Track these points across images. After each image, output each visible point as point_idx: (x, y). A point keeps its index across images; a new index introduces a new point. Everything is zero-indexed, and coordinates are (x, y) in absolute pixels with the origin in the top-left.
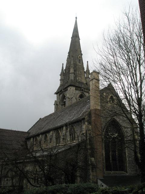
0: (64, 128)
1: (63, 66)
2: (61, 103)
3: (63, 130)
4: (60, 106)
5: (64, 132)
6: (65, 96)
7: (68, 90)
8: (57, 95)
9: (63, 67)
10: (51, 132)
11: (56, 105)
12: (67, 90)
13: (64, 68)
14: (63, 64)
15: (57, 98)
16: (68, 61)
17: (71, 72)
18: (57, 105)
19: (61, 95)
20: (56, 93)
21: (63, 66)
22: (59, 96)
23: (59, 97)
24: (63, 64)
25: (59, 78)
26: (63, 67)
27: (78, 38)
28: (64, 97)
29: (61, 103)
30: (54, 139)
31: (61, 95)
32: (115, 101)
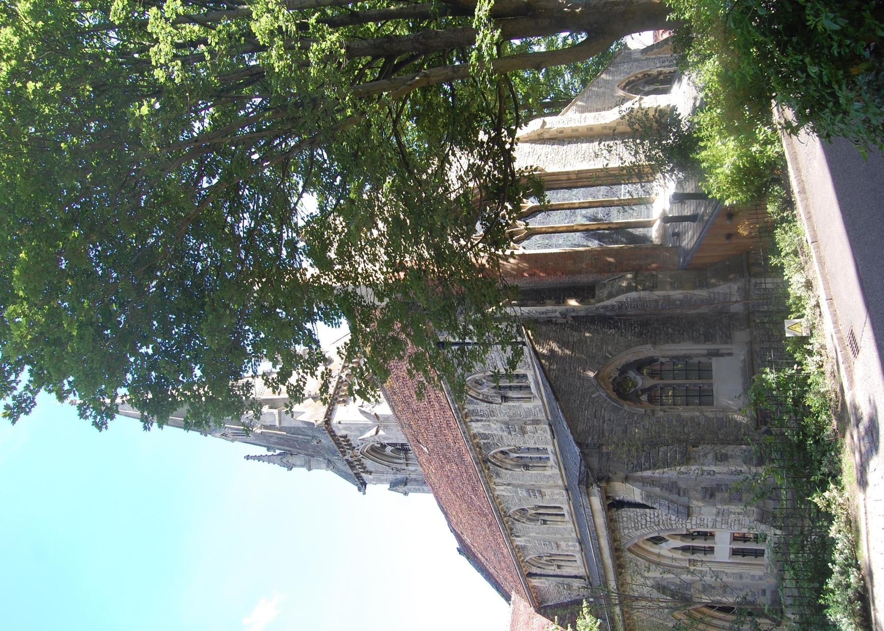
0: (476, 427)
1: (255, 458)
2: (399, 466)
3: (485, 436)
4: (411, 468)
5: (495, 429)
6: (373, 449)
7: (344, 433)
8: (370, 483)
9: (259, 458)
10: (500, 491)
11: (408, 486)
12: (345, 437)
13: (262, 451)
14: (248, 457)
15: (380, 481)
16: (235, 434)
17: (630, 197)
18: (405, 482)
19: (368, 463)
20: (362, 485)
21: (255, 458)
22: (371, 473)
23: (377, 472)
24: (248, 457)
25: (299, 472)
26: (259, 458)
27: (769, 283)
28: (377, 451)
29: (399, 466)
30: (530, 477)
31: (368, 463)
32: (381, 225)
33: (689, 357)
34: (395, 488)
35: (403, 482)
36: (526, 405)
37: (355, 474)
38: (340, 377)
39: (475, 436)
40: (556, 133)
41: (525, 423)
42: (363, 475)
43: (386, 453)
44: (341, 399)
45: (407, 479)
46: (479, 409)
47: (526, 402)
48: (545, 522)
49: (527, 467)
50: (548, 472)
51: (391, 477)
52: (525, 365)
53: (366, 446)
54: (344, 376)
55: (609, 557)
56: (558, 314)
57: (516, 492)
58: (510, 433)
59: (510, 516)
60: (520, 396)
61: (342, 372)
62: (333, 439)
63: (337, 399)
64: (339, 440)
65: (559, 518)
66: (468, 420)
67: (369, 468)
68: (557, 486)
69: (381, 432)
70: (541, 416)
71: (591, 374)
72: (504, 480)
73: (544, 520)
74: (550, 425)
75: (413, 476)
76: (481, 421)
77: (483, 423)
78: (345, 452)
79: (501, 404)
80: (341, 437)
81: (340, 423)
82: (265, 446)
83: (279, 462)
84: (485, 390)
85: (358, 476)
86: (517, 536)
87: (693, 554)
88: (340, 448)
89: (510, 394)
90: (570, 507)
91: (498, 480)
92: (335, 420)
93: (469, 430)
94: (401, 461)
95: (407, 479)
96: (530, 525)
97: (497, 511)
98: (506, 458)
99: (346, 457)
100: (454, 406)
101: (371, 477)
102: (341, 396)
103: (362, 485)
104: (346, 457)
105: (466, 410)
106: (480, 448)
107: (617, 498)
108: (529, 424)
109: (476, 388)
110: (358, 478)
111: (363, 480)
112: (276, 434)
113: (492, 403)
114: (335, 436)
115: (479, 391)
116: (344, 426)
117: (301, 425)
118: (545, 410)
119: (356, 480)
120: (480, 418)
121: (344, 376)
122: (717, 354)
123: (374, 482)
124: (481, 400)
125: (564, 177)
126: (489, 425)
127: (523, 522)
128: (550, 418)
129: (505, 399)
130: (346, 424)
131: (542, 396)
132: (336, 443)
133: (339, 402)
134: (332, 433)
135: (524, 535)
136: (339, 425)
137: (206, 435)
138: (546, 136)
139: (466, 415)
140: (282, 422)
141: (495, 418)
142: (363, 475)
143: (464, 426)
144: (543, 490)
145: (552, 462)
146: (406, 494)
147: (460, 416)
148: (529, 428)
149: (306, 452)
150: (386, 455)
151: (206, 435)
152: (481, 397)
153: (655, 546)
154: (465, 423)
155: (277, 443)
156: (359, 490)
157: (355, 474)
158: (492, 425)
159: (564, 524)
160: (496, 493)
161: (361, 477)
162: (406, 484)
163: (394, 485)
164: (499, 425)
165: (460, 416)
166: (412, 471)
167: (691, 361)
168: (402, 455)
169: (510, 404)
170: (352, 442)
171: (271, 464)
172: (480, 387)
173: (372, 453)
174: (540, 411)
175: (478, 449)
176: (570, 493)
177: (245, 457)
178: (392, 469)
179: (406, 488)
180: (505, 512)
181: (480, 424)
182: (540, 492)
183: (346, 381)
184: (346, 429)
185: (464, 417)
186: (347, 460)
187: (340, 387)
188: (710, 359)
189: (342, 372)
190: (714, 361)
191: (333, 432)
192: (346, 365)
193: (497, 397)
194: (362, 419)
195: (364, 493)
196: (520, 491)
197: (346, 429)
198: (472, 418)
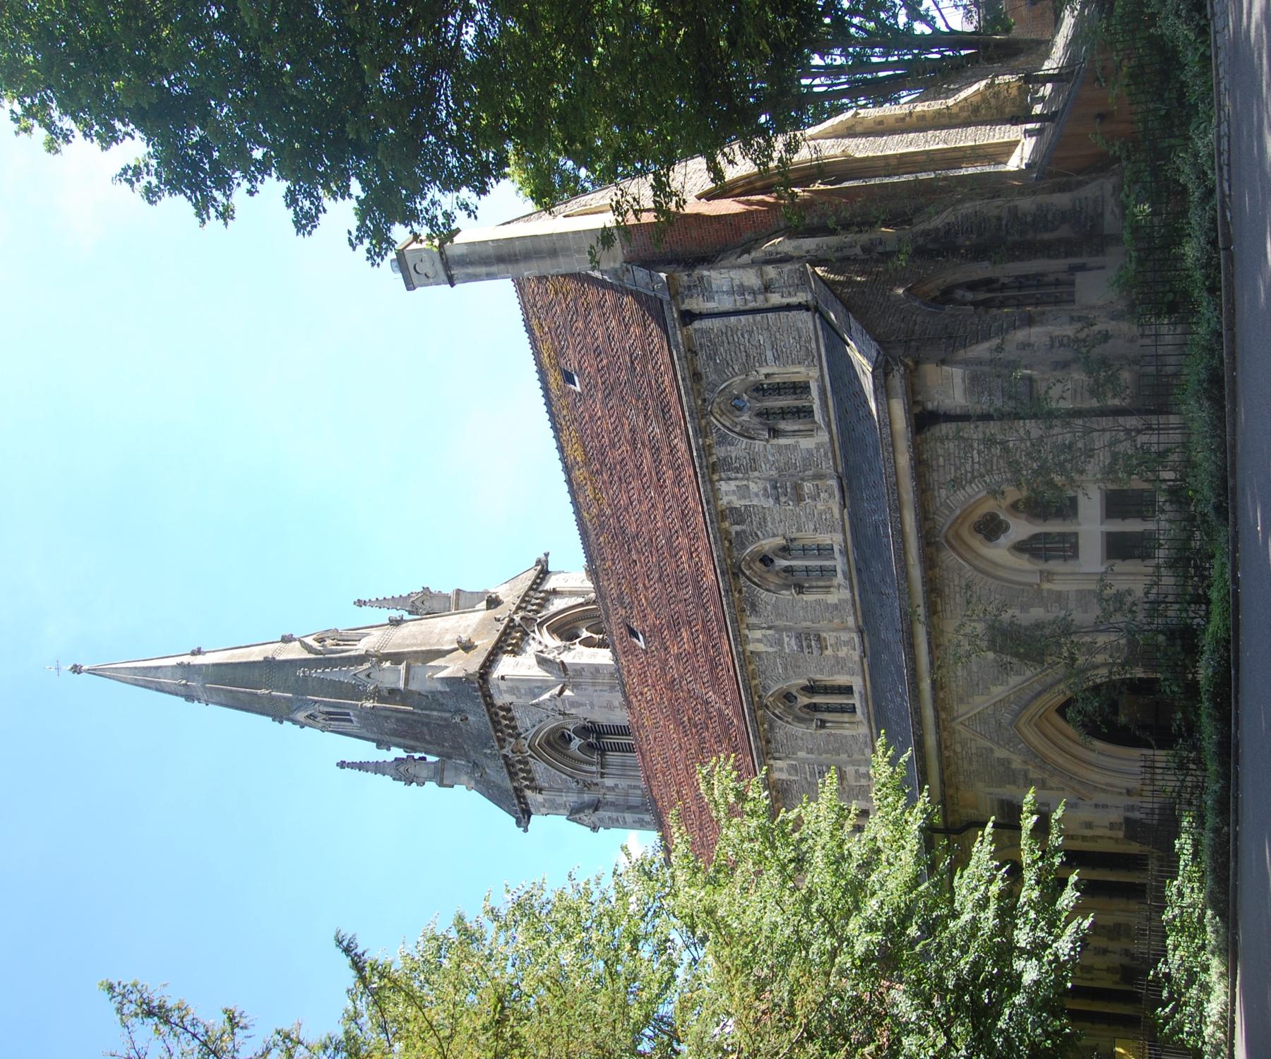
4: (609, 782)
8: (538, 812)
10: (758, 641)
13: (366, 750)
14: (342, 765)
18: (596, 806)
19: (539, 769)
20: (523, 815)
22: (540, 790)
23: (551, 788)
24: (342, 765)
31: (539, 769)
33: (1043, 275)
34: (577, 816)
35: (592, 805)
36: (806, 443)
37: (515, 788)
38: (512, 620)
39: (722, 515)
40: (873, 125)
41: (802, 479)
42: (528, 793)
43: (568, 752)
44: (510, 648)
45: (599, 801)
46: (733, 455)
47: (806, 436)
48: (823, 724)
49: (800, 589)
50: (832, 598)
51: (572, 798)
52: (808, 356)
53: (538, 732)
54: (517, 618)
55: (917, 562)
56: (858, 250)
57: (780, 642)
58: (777, 500)
59: (767, 706)
60: (796, 428)
61: (515, 612)
62: (488, 710)
63: (502, 647)
64: (497, 714)
65: (846, 717)
66: (715, 477)
67: (540, 782)
68: (846, 629)
69: (567, 693)
70: (827, 466)
71: (900, 291)
72: (762, 619)
73: (821, 720)
74: (840, 478)
75: (610, 797)
76: (736, 479)
77: (738, 483)
78: (504, 740)
79: (767, 441)
80: (501, 708)
81: (503, 678)
82: (373, 740)
83: (393, 772)
84: (745, 418)
85: (519, 793)
86: (775, 759)
87: (1046, 560)
88: (497, 731)
89: (783, 425)
90: (864, 680)
91: (753, 620)
92: (496, 674)
93: (716, 499)
94: (594, 768)
95: (599, 801)
96: (799, 729)
97: (748, 688)
98: (768, 571)
99: (504, 752)
100: (697, 443)
101: (540, 798)
102: (509, 645)
103: (523, 815)
104: (504, 752)
105: (714, 459)
106: (730, 542)
107: (930, 406)
108: (807, 480)
109: (731, 413)
110: (518, 797)
111: (526, 804)
112: (397, 711)
113: (754, 439)
114: (493, 705)
115: (736, 420)
116: (510, 684)
117: (440, 687)
118: (834, 452)
119: (516, 802)
120: (734, 475)
121: (517, 618)
122: (1082, 268)
123: (544, 810)
124: (738, 434)
125: (882, 163)
126: (747, 487)
127: (787, 722)
128: (840, 470)
129: (775, 433)
130: (512, 680)
131: (829, 419)
132: (491, 719)
133: (505, 652)
134: (487, 696)
135: (787, 757)
136: (501, 682)
137: (281, 722)
138: (859, 129)
139: (714, 468)
140: (411, 682)
141: (756, 474)
142: (528, 793)
143: (709, 487)
144: (824, 635)
145: (840, 579)
146: (595, 829)
147: (705, 463)
148: (808, 487)
149: (439, 750)
150: (568, 756)
151: (281, 722)
152: (737, 430)
153: (989, 544)
154: (712, 482)
155: (395, 733)
156: (518, 823)
157: (515, 788)
158: (752, 485)
159: (855, 726)
160: (751, 647)
161: (524, 797)
162: (596, 809)
163: (575, 813)
164: (761, 484)
165: (705, 463)
166: (609, 788)
167: (1045, 279)
168: (596, 758)
169: (782, 441)
170: (518, 723)
171: (379, 775)
172: (738, 413)
173: (548, 749)
174: (826, 454)
175: (727, 544)
176: (865, 636)
177: (338, 764)
178: (577, 782)
179: (594, 818)
180: (760, 697)
181: (733, 483)
182: (819, 638)
183: (520, 625)
184: (512, 691)
185: (712, 469)
186: (505, 757)
187: (510, 634)
188: (1073, 275)
189: (515, 612)
190: (1079, 277)
191: (491, 696)
192: (524, 605)
193: (763, 430)
194: (538, 672)
195: (526, 830)
196: (786, 639)
197: (512, 691)
198: (723, 475)
